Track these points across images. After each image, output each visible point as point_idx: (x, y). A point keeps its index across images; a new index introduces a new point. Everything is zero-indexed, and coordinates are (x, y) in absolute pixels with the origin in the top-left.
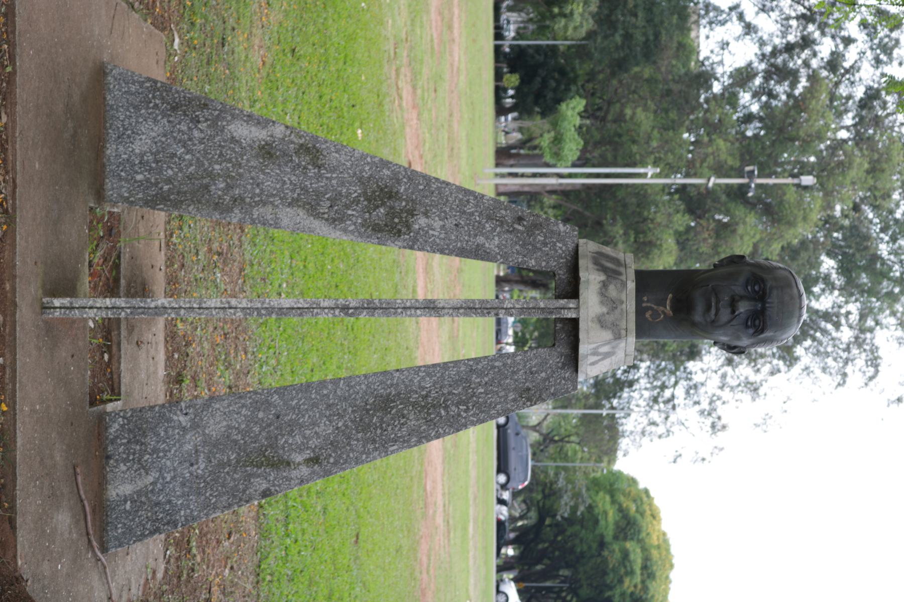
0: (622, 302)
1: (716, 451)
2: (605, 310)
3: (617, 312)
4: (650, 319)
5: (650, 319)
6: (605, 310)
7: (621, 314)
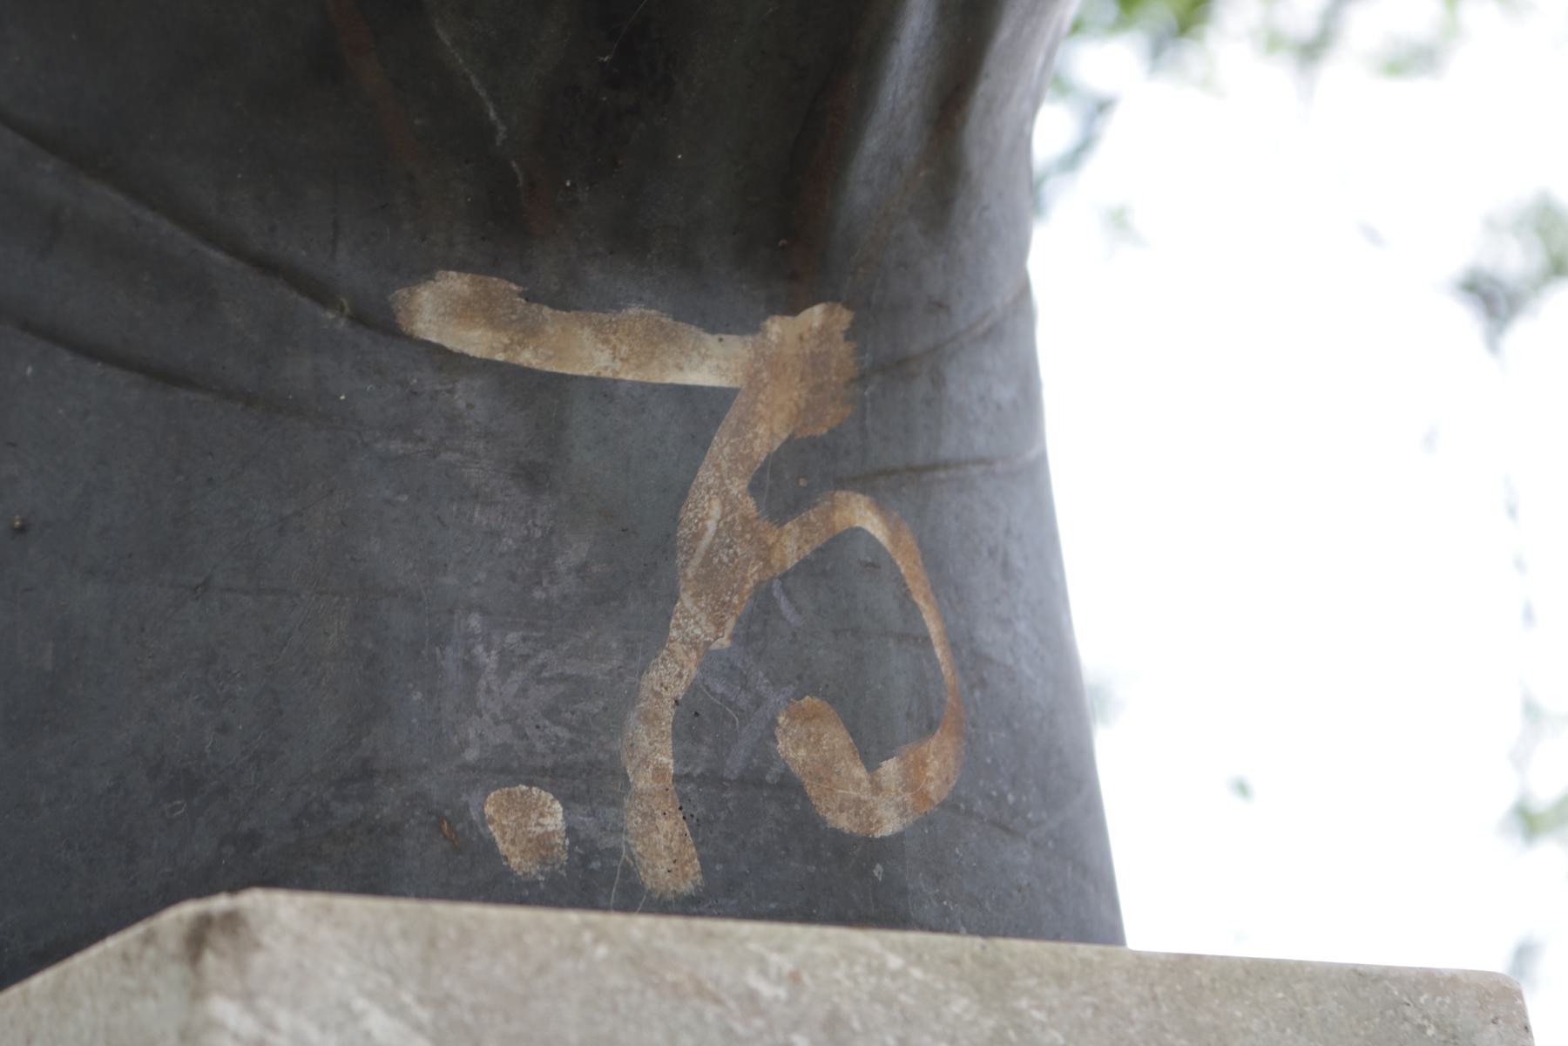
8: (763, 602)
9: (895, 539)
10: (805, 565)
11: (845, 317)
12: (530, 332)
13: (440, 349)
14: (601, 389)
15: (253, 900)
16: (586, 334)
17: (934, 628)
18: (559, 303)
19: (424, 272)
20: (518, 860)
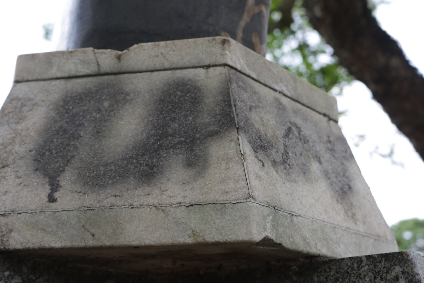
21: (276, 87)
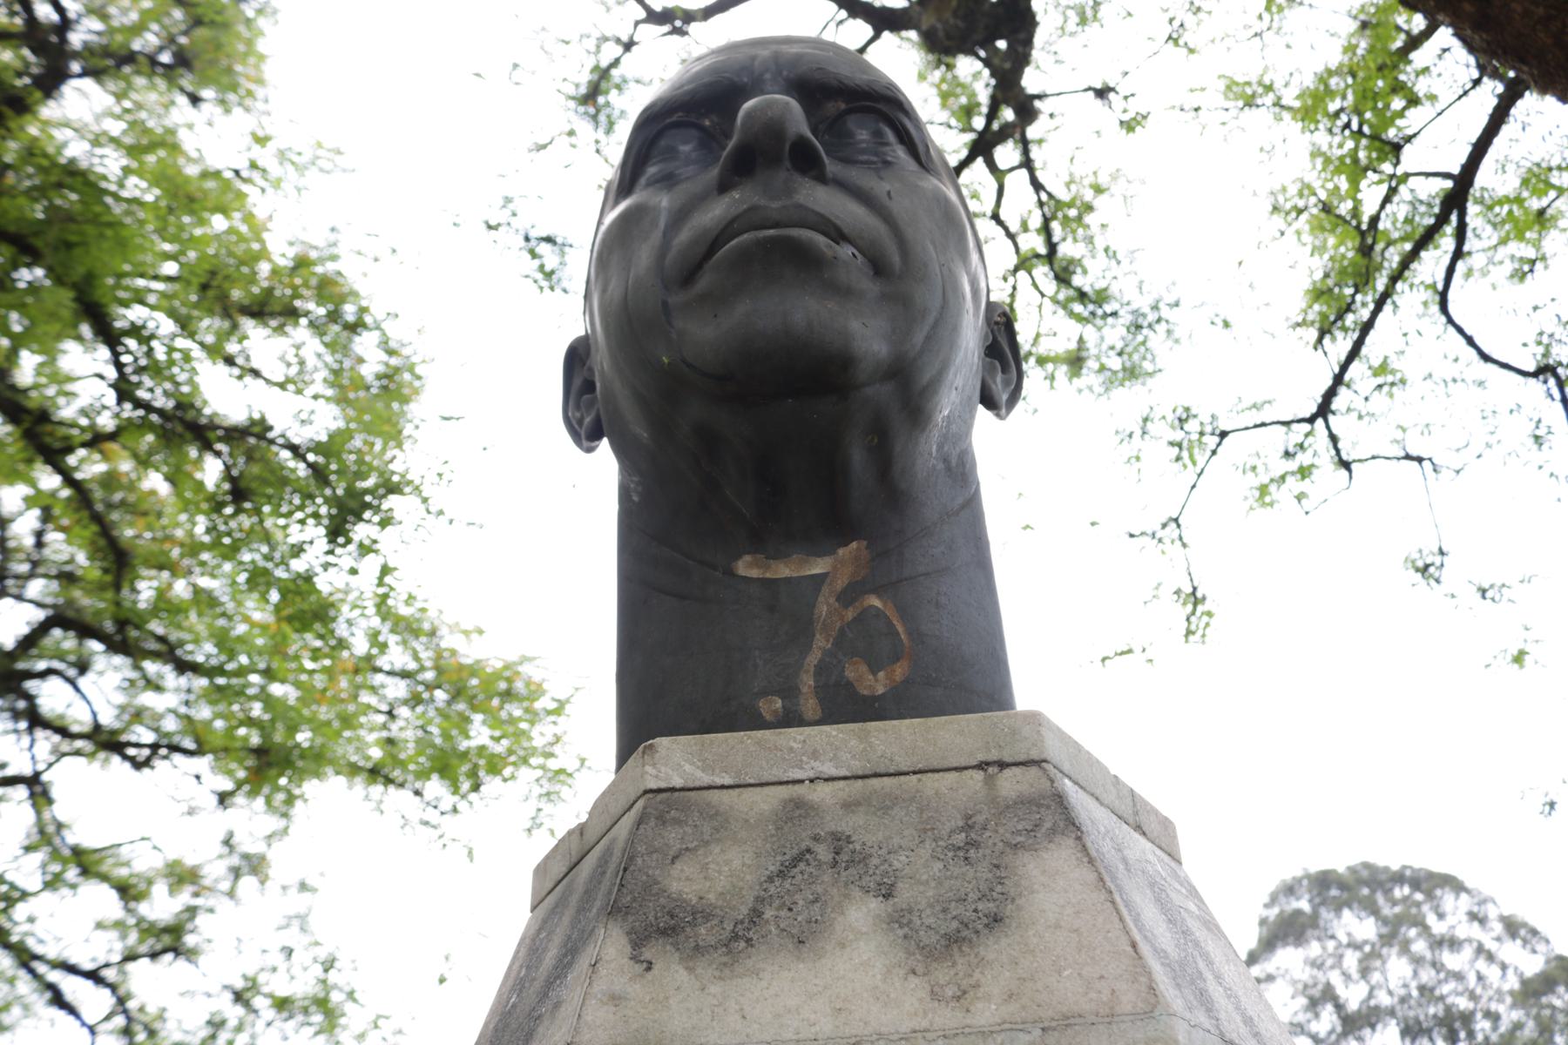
0: (798, 809)
1: (1513, 143)
2: (861, 913)
3: (864, 829)
4: (900, 671)
5: (900, 671)
6: (861, 913)
7: (885, 805)
8: (842, 632)
9: (885, 604)
10: (855, 619)
11: (865, 543)
12: (768, 568)
13: (745, 578)
14: (788, 580)
15: (658, 740)
16: (782, 566)
17: (900, 629)
18: (775, 558)
19: (738, 557)
20: (768, 717)
21: (799, 775)
